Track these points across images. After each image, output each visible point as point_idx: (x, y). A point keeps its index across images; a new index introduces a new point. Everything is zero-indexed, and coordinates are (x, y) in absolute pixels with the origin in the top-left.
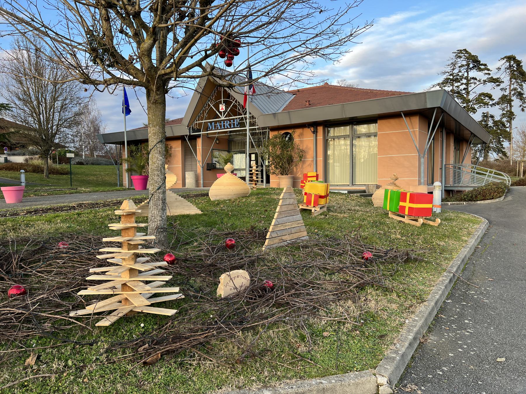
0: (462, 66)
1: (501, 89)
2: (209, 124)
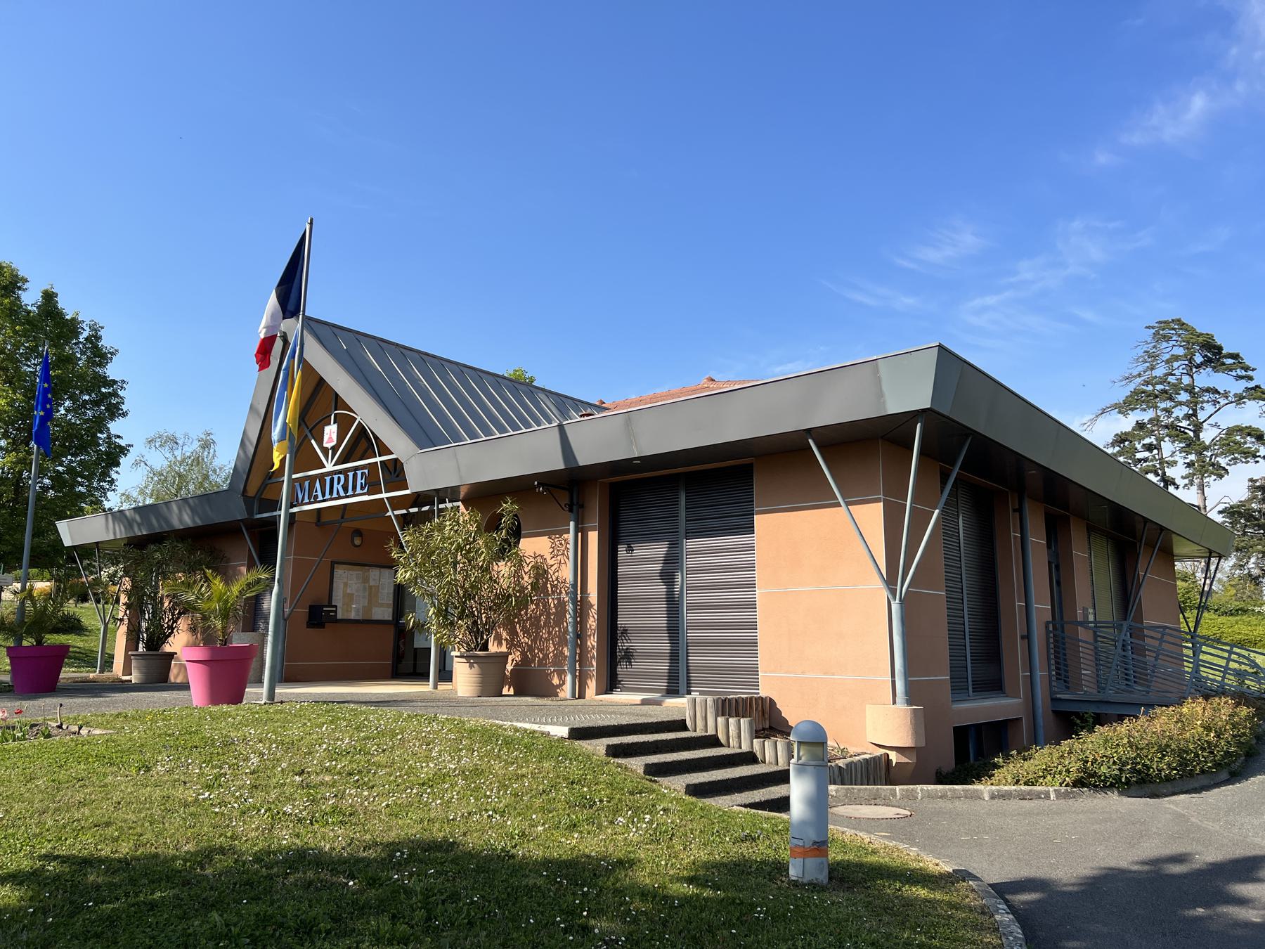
0: (1176, 358)
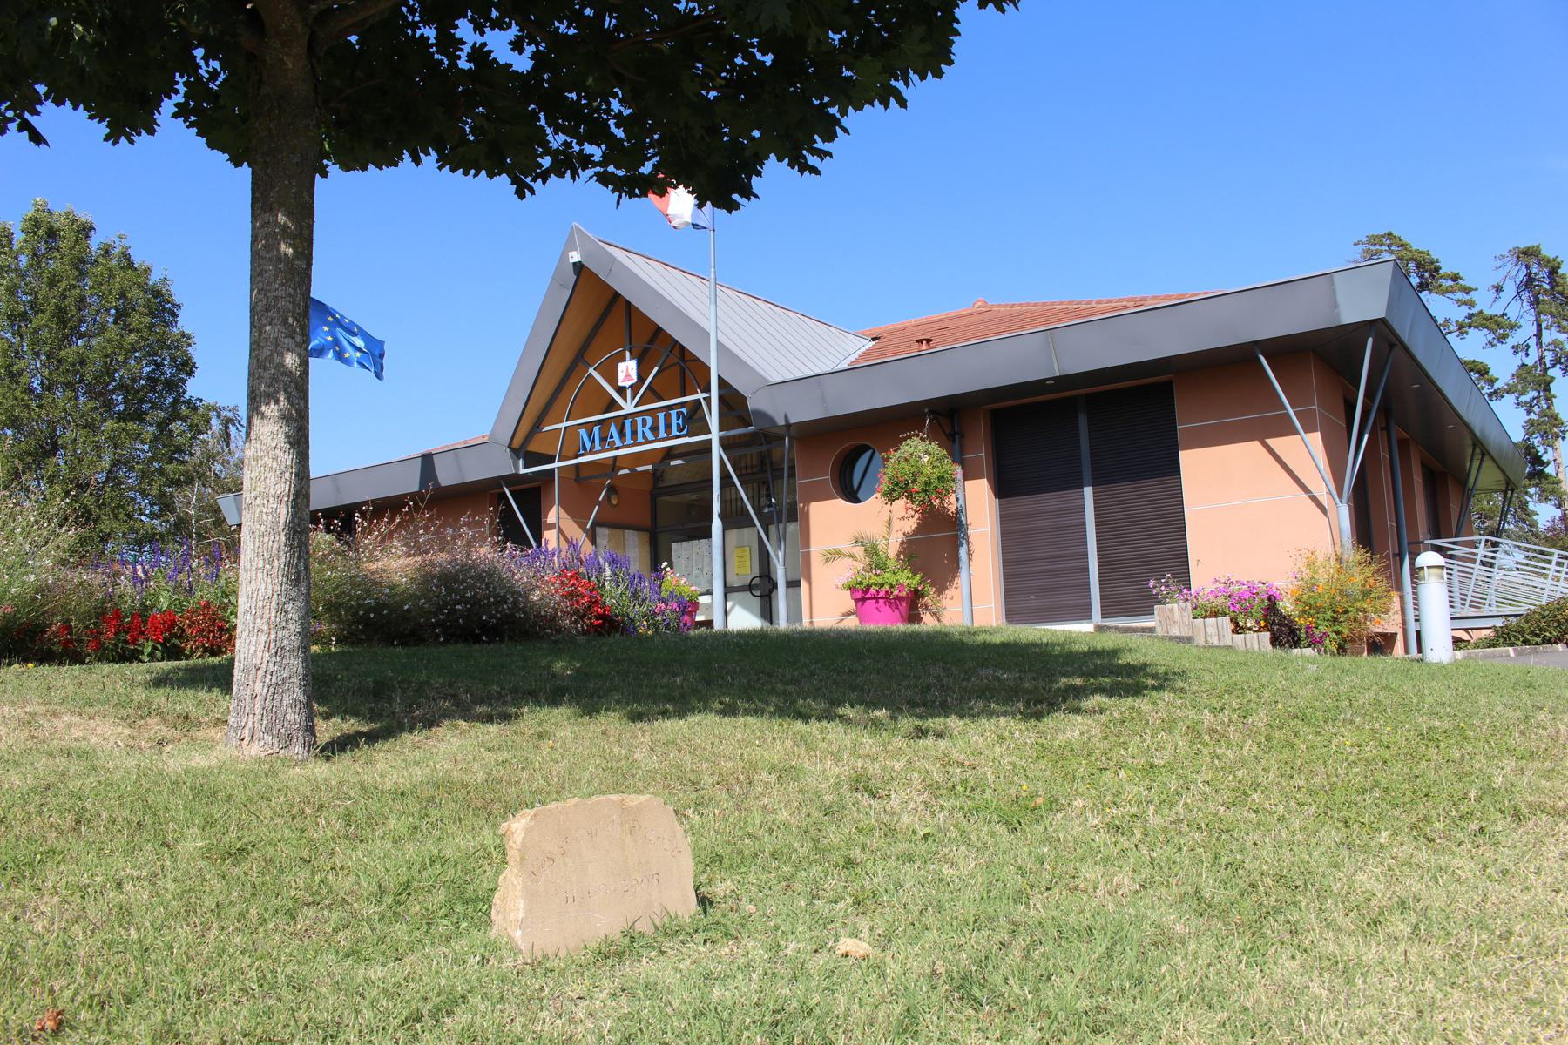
1: (1516, 349)
2: (583, 432)
